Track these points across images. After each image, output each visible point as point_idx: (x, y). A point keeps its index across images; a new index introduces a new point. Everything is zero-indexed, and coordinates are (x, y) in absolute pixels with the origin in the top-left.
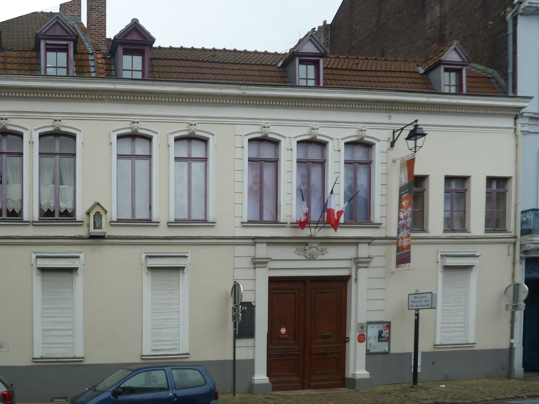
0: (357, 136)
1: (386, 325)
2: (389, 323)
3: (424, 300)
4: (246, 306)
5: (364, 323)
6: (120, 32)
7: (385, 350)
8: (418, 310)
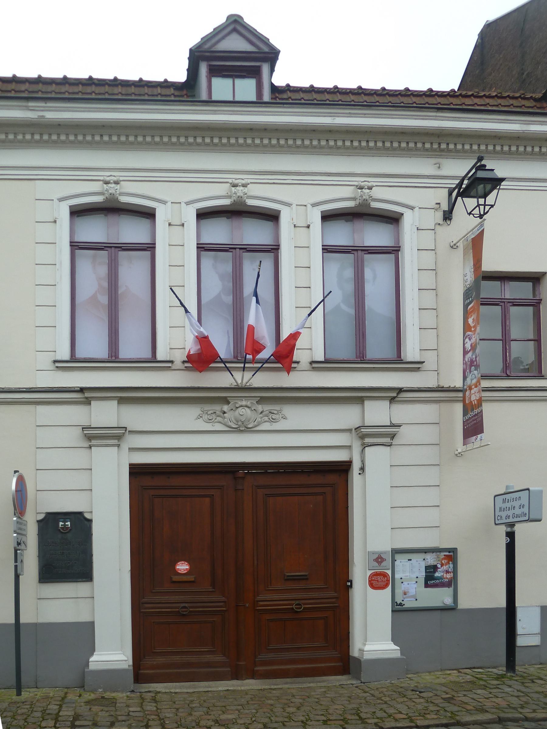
0: (354, 199)
1: (444, 555)
2: (454, 551)
3: (517, 504)
4: (68, 520)
5: (385, 553)
6: (214, 29)
7: (445, 604)
8: (512, 525)
